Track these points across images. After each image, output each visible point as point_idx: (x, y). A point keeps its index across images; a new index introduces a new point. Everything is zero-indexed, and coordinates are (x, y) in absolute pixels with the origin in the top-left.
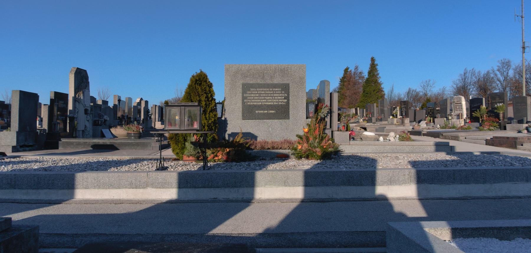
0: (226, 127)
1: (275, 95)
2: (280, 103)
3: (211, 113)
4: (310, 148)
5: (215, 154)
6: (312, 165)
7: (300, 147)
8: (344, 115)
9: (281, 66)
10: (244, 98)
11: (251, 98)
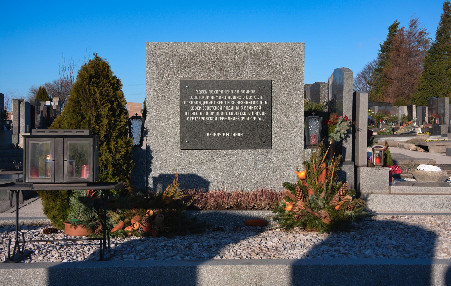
0: (150, 163)
1: (244, 102)
2: (254, 119)
3: (119, 140)
4: (309, 210)
5: (127, 220)
6: (310, 245)
7: (289, 208)
8: (386, 118)
9: (256, 47)
10: (183, 109)
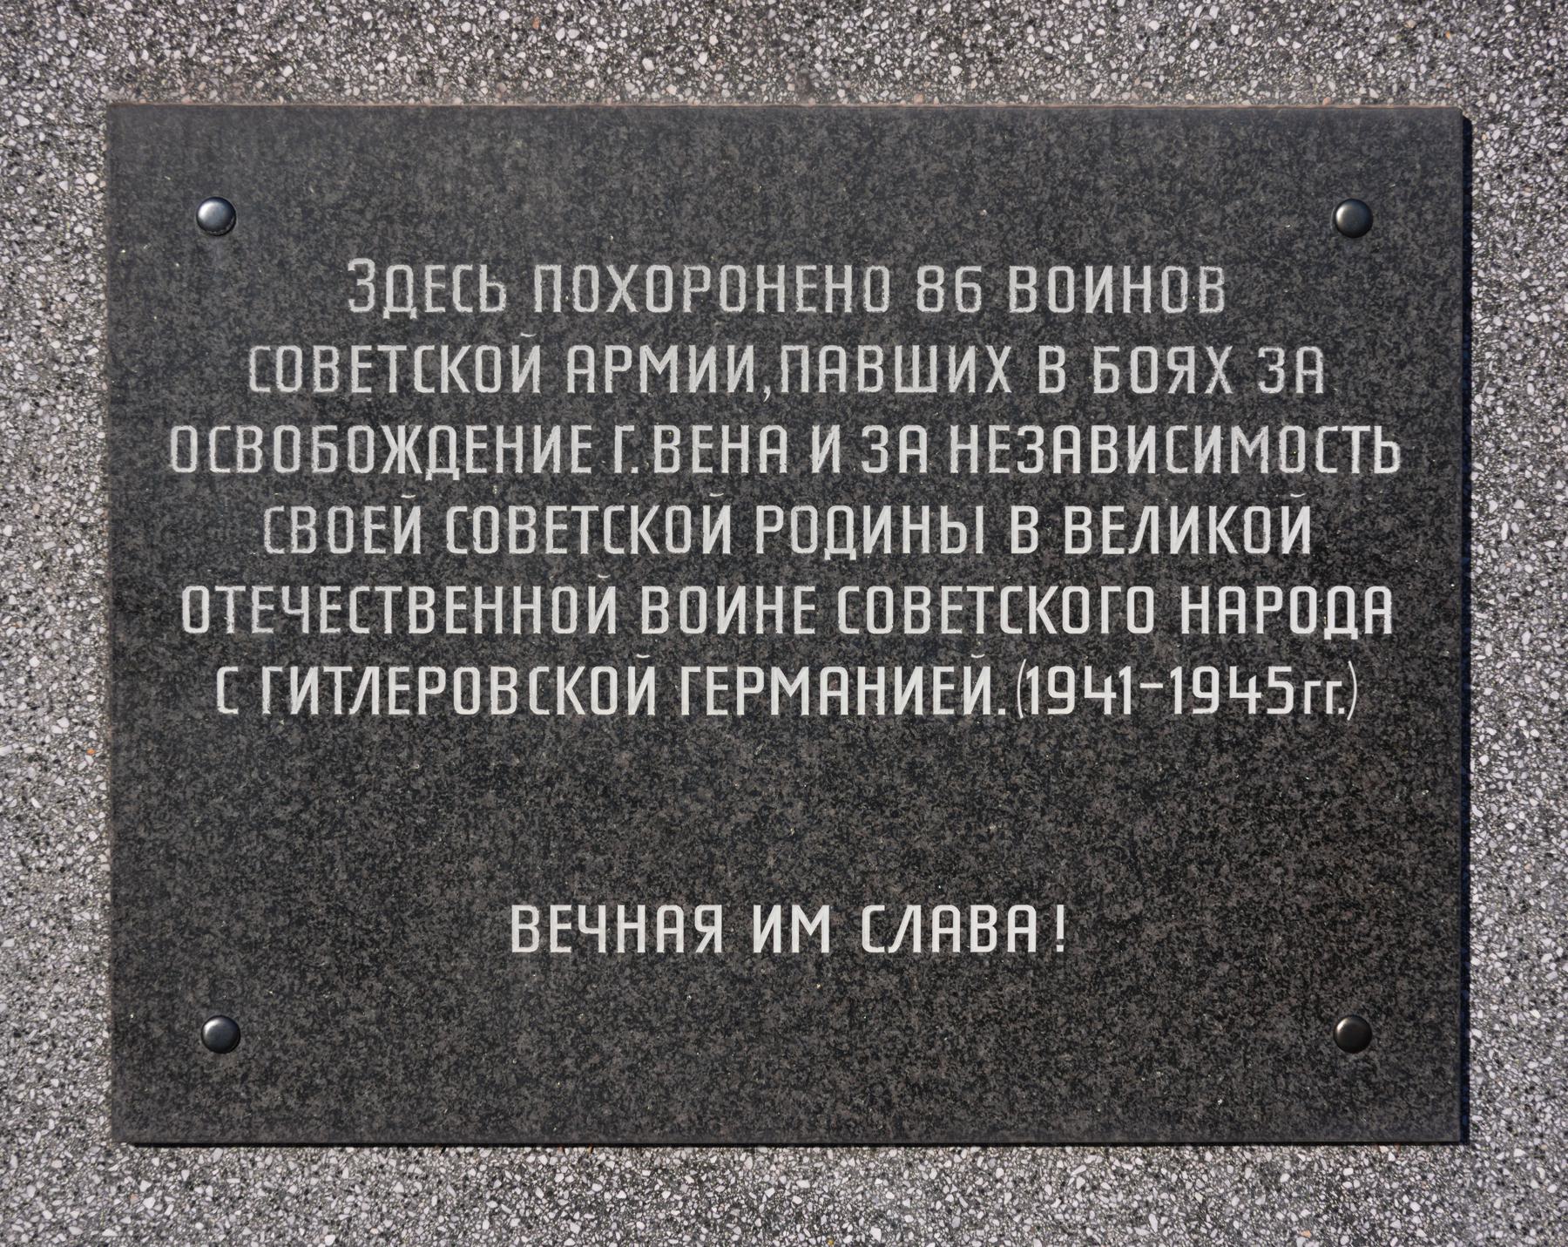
1: (1057, 449)
2: (1205, 691)
10: (157, 540)
11: (355, 530)
